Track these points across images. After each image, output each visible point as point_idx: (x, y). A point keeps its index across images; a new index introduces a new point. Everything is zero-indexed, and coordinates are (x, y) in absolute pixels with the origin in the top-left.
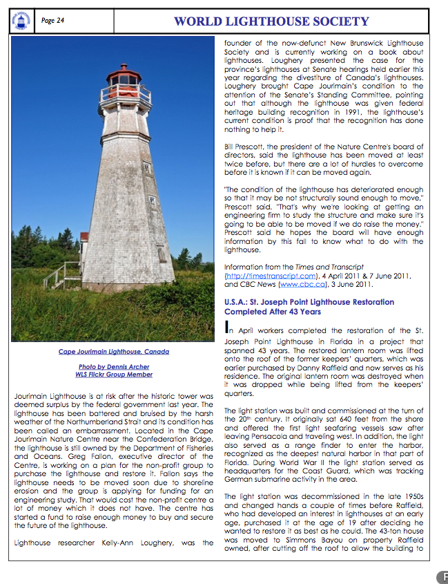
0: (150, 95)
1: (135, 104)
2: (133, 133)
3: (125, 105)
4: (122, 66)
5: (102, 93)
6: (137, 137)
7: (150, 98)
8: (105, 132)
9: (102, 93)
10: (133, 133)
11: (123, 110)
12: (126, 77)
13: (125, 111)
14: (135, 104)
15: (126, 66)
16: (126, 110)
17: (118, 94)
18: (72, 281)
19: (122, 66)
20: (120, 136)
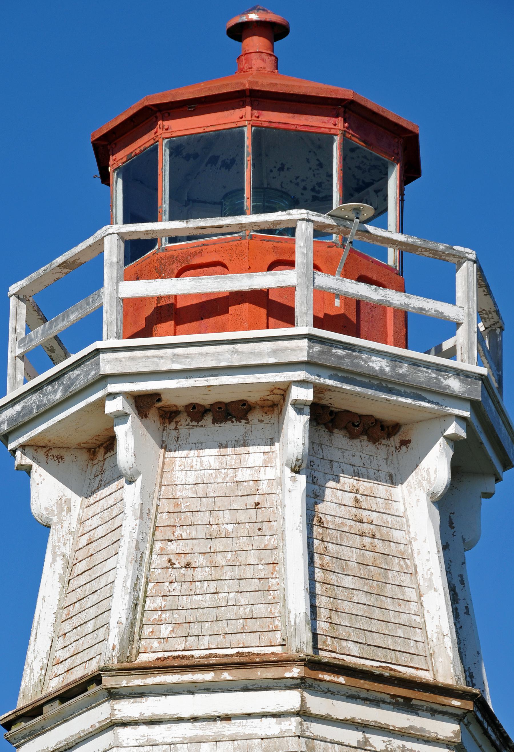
0: (465, 278)
1: (274, 403)
2: (244, 669)
3: (197, 412)
4: (239, 32)
5: (18, 313)
6: (291, 699)
7: (462, 306)
8: (39, 675)
9: (18, 313)
10: (244, 669)
11: (182, 458)
12: (235, 137)
13: (199, 466)
14: (274, 403)
15: (275, 31)
16: (210, 456)
17: (111, 317)
18: (401, 289)
19: (239, 32)
20: (126, 709)
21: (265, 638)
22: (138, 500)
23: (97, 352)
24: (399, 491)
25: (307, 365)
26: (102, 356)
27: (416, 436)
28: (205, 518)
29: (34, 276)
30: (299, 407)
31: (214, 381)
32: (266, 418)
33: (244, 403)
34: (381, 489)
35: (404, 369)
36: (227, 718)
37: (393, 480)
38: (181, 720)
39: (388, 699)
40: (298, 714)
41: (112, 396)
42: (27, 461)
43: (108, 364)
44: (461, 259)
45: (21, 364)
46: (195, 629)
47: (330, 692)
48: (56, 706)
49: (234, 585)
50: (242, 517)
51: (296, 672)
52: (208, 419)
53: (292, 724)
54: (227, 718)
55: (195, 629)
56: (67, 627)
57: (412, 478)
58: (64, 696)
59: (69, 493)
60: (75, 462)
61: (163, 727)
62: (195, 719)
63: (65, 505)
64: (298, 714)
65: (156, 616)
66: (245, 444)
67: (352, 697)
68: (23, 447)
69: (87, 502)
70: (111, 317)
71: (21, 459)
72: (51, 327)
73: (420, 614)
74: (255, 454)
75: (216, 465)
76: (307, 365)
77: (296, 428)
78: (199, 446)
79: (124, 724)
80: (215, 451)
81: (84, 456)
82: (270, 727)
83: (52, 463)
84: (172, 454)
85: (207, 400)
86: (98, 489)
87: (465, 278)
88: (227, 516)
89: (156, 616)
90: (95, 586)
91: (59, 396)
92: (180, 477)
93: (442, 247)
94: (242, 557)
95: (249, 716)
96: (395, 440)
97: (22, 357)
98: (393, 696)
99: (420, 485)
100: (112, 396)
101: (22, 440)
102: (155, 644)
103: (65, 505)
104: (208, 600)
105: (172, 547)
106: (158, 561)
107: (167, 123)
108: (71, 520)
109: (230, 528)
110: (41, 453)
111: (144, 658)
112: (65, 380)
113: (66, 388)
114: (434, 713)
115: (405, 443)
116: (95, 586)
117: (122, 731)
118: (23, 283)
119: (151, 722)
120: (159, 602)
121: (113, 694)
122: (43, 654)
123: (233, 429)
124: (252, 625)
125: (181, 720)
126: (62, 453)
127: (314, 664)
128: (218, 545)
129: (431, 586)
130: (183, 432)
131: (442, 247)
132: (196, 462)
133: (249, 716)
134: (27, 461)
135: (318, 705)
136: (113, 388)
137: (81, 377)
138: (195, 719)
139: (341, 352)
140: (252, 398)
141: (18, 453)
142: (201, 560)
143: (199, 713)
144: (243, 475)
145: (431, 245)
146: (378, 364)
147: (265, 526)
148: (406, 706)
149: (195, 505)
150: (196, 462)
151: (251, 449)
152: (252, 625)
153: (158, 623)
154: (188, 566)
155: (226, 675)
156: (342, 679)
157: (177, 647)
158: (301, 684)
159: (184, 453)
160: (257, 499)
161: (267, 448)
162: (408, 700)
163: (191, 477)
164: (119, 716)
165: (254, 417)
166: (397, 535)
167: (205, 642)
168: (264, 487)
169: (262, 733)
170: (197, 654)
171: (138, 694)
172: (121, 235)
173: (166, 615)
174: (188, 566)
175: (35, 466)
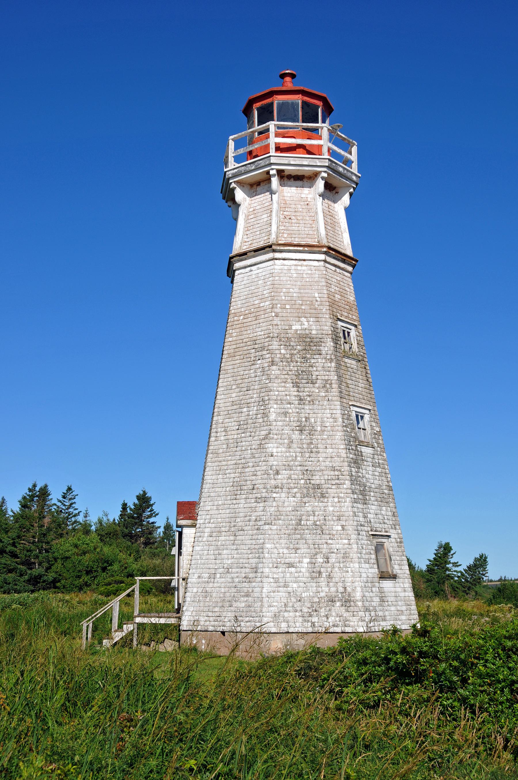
0: (354, 150)
6: (322, 257)
7: (354, 157)
10: (311, 248)
11: (286, 189)
13: (291, 192)
15: (293, 76)
16: (293, 189)
17: (272, 147)
20: (277, 255)
21: (313, 240)
22: (277, 199)
23: (270, 156)
24: (336, 205)
25: (327, 167)
26: (271, 157)
27: (340, 191)
28: (294, 206)
29: (240, 134)
30: (323, 178)
31: (301, 168)
32: (308, 181)
33: (304, 176)
34: (332, 204)
35: (345, 172)
36: (304, 260)
37: (335, 202)
38: (292, 260)
39: (341, 259)
40: (323, 261)
41: (273, 169)
42: (235, 186)
43: (273, 160)
44: (354, 144)
45: (233, 159)
46: (294, 236)
47: (330, 256)
48: (253, 253)
49: (303, 225)
50: (304, 207)
51: (325, 249)
52: (292, 180)
53: (322, 263)
54: (304, 260)
55: (294, 236)
56: (248, 232)
57: (339, 202)
58: (256, 251)
59: (246, 196)
60: (247, 188)
61: (287, 261)
62: (296, 260)
63: (245, 199)
64: (323, 261)
65: (282, 231)
66: (303, 187)
67: (334, 258)
68: (234, 182)
69: (251, 199)
70: (272, 147)
71: (233, 185)
72: (247, 149)
73: (342, 238)
74: (306, 190)
75: (295, 192)
76: (327, 167)
77: (320, 185)
78: (290, 186)
79: (276, 259)
80: (295, 188)
81: (249, 187)
82: (316, 263)
83: (241, 187)
84: (283, 188)
85: (293, 174)
86: (255, 196)
87: (354, 150)
88: (300, 206)
89: (282, 231)
90: (258, 222)
91: (253, 168)
92: (286, 194)
93: (351, 140)
94: (305, 218)
95: (311, 260)
96: (334, 192)
97: (234, 157)
98: (342, 259)
99: (342, 204)
100: (273, 169)
101: (235, 180)
102: (283, 239)
103: (245, 199)
104: (296, 228)
105: (285, 213)
106: (282, 217)
107: (277, 96)
108: (246, 204)
109: (301, 210)
110: (239, 184)
111: (280, 242)
112: (256, 164)
113: (256, 166)
114: (349, 264)
115: (337, 193)
116: (258, 222)
117: (276, 261)
118: (236, 136)
119: (284, 259)
120: (283, 228)
121: (274, 251)
122: (241, 239)
123: (299, 183)
124: (310, 236)
125: (292, 260)
126: (244, 185)
127: (329, 248)
128: (298, 214)
129: (345, 231)
130: (286, 182)
131: (351, 140)
132: (290, 191)
133: (311, 260)
134: (235, 186)
135: (329, 259)
136: (273, 167)
137: (262, 163)
138: (296, 260)
139: (334, 165)
140: (306, 174)
141: (233, 183)
142: (293, 218)
143: (298, 258)
144: (303, 196)
145: (349, 139)
146: (341, 169)
147: (310, 210)
148: (344, 261)
149: (291, 202)
150: (290, 191)
151: (305, 189)
152: (310, 236)
153: (283, 233)
154: (290, 219)
155: (306, 249)
156: (334, 253)
157: (289, 240)
158: (325, 253)
159: (286, 188)
160: (307, 202)
161: (309, 189)
162: (345, 260)
163: (289, 195)
164: (276, 257)
165: (305, 180)
166: (336, 217)
167: (297, 239)
168: (309, 200)
169: (314, 265)
170: (295, 242)
171: (281, 251)
172: (275, 125)
173: (285, 231)
174: (290, 219)
175: (237, 187)
